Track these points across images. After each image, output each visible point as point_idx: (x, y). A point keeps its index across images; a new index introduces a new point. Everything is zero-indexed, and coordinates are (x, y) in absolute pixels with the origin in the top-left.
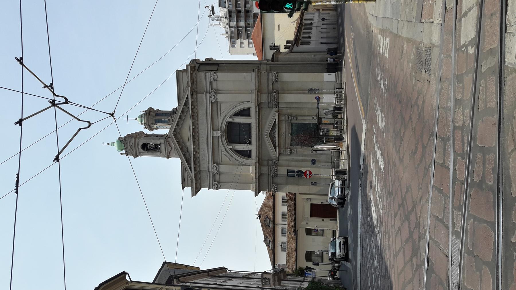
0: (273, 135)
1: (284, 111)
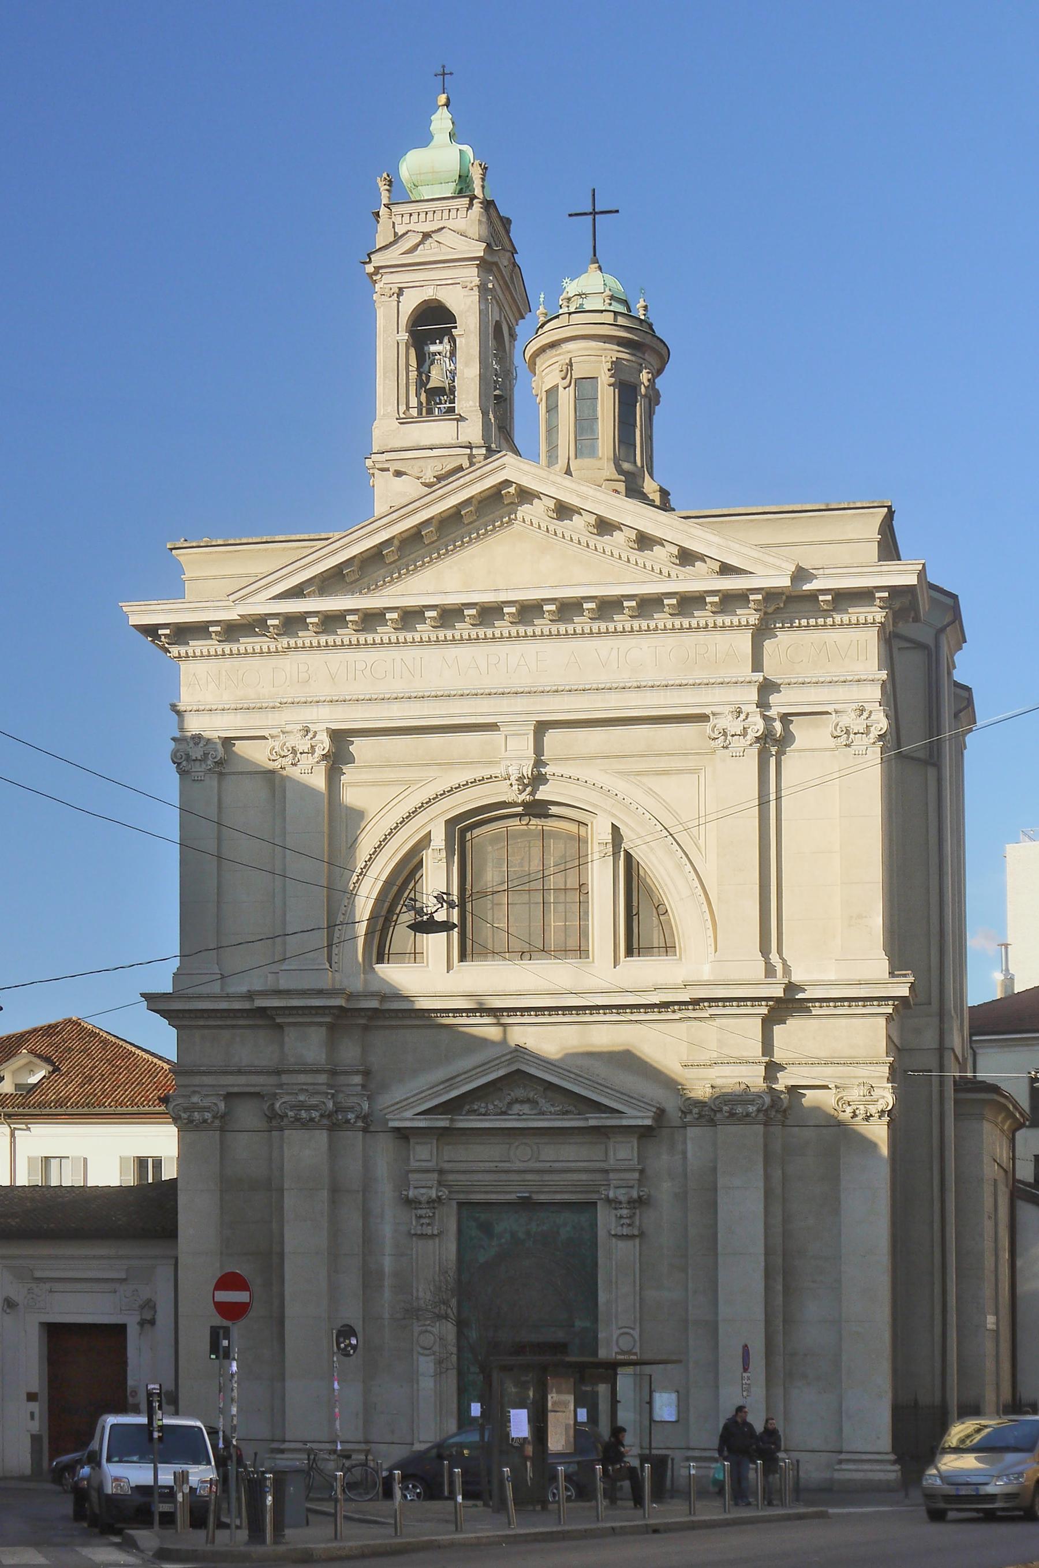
0: (520, 1093)
1: (662, 1160)
